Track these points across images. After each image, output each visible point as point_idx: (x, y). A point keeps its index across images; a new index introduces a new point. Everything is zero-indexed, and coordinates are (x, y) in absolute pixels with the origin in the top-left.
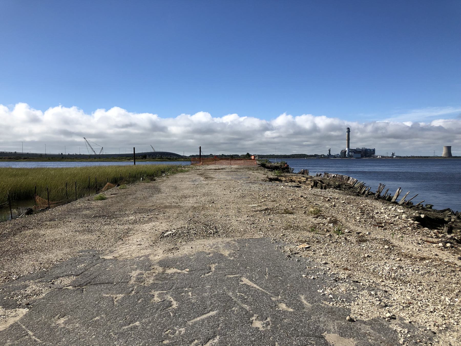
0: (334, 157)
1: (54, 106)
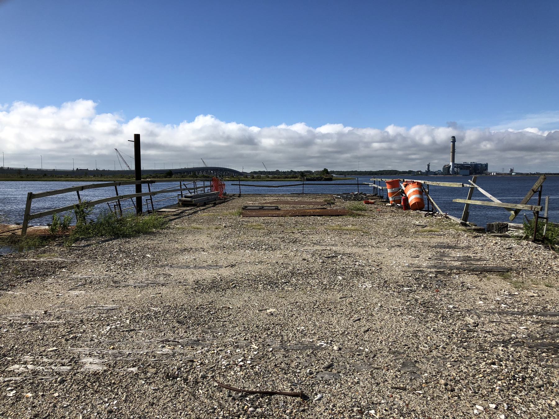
0: (435, 173)
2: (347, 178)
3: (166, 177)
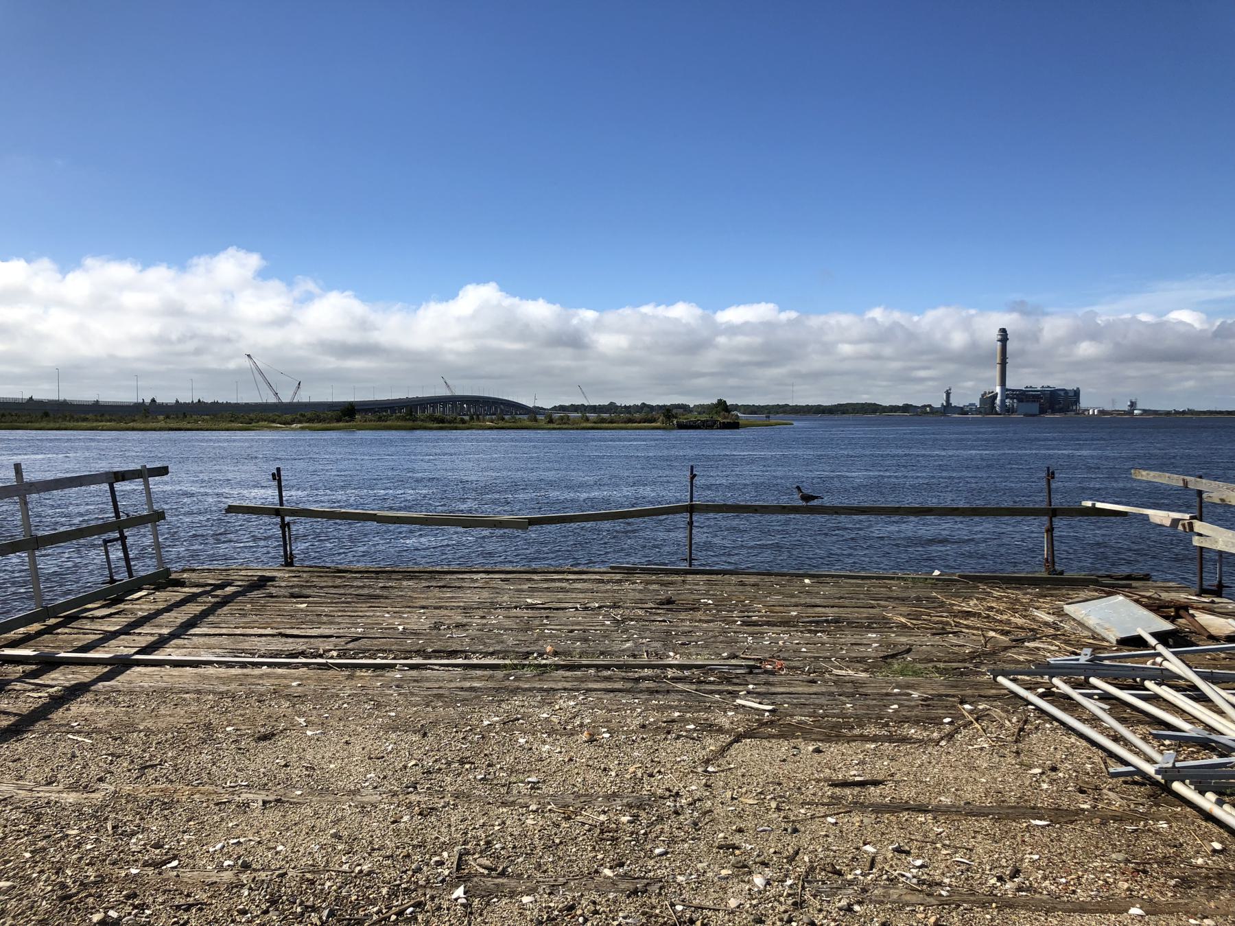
0: (962, 411)
1: (934, 307)
2: (772, 421)
3: (338, 421)
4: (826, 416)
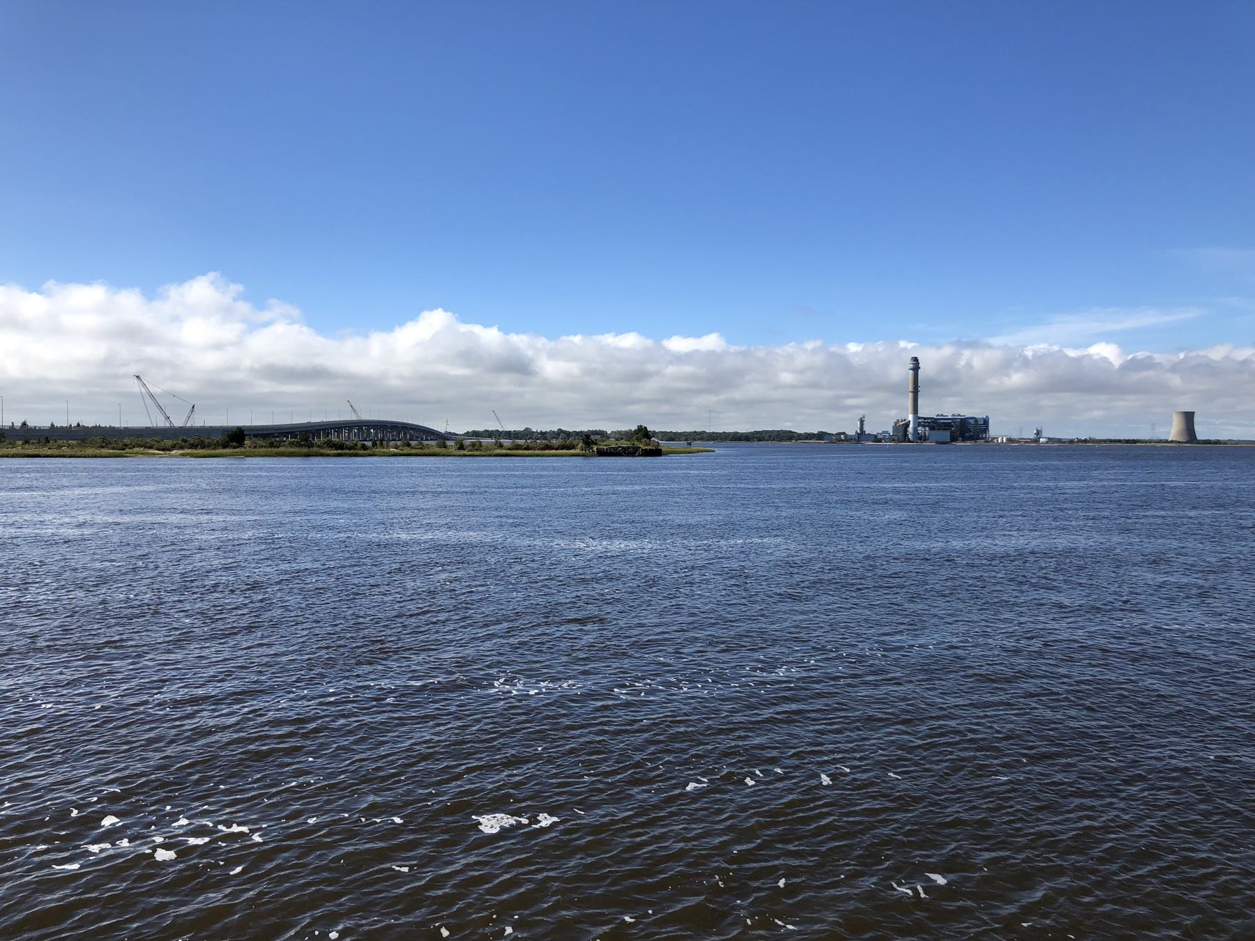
0: (876, 439)
2: (694, 448)
3: (225, 447)
4: (743, 443)
